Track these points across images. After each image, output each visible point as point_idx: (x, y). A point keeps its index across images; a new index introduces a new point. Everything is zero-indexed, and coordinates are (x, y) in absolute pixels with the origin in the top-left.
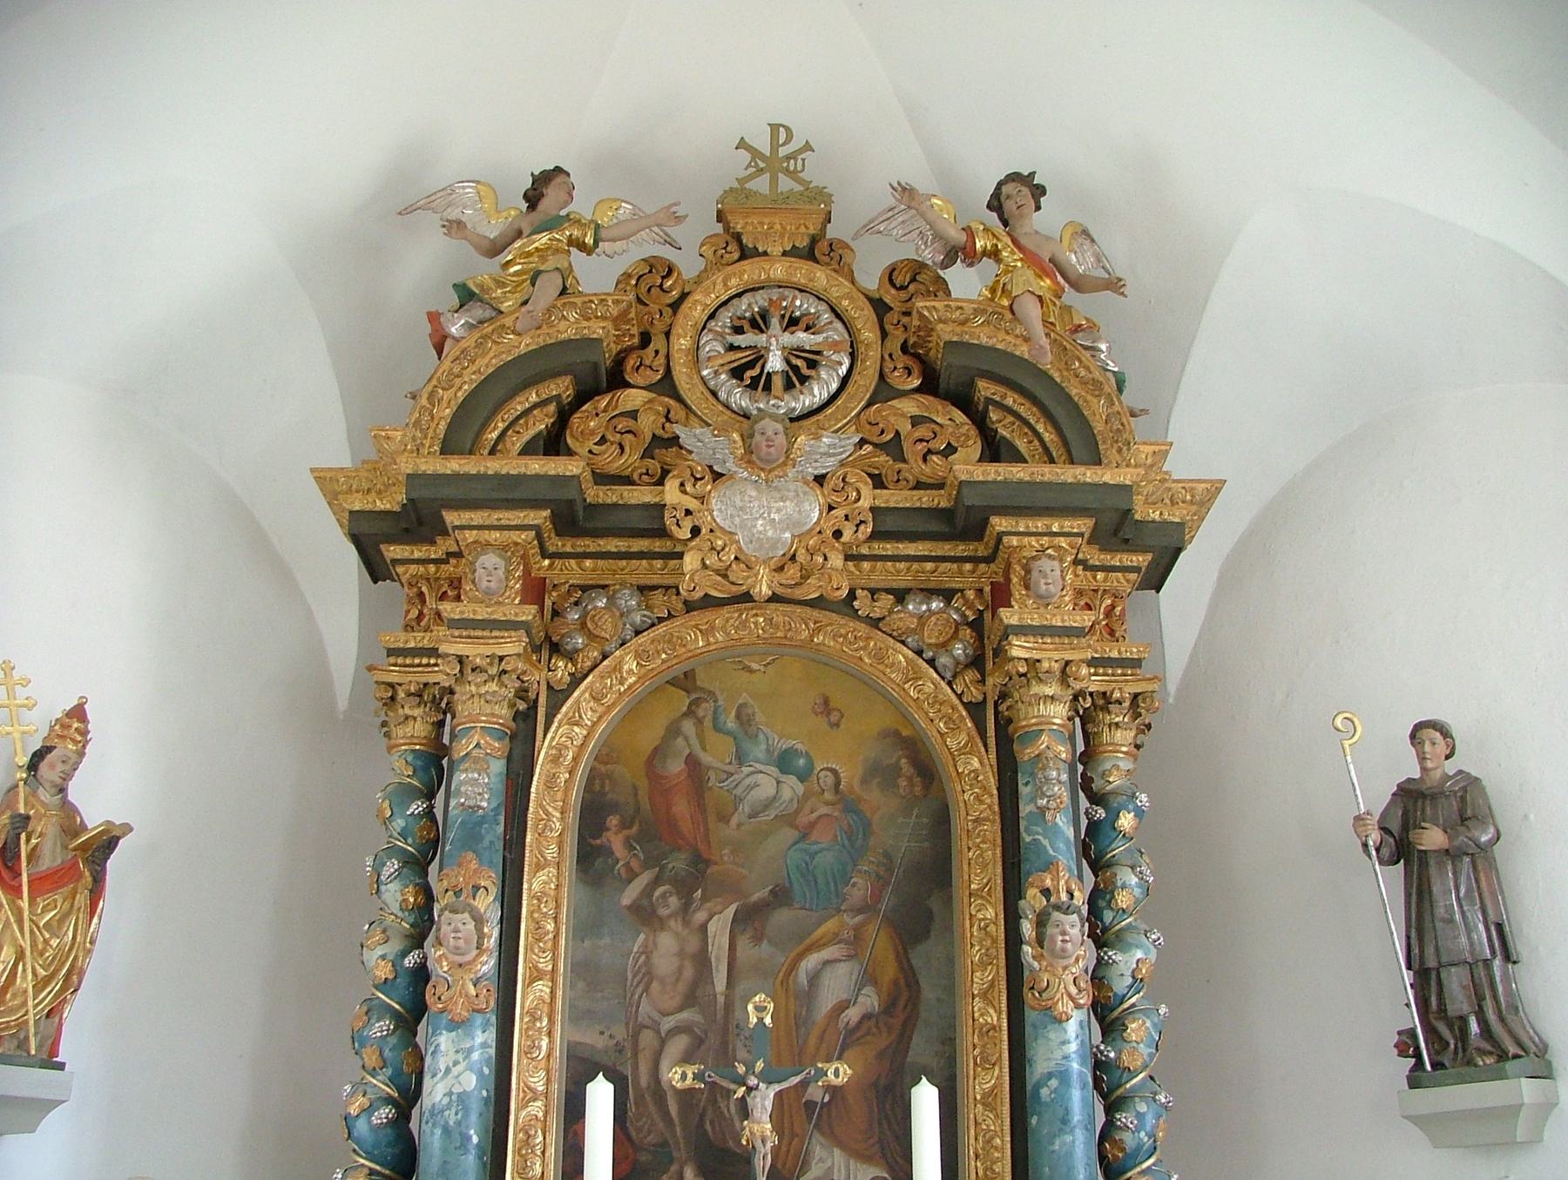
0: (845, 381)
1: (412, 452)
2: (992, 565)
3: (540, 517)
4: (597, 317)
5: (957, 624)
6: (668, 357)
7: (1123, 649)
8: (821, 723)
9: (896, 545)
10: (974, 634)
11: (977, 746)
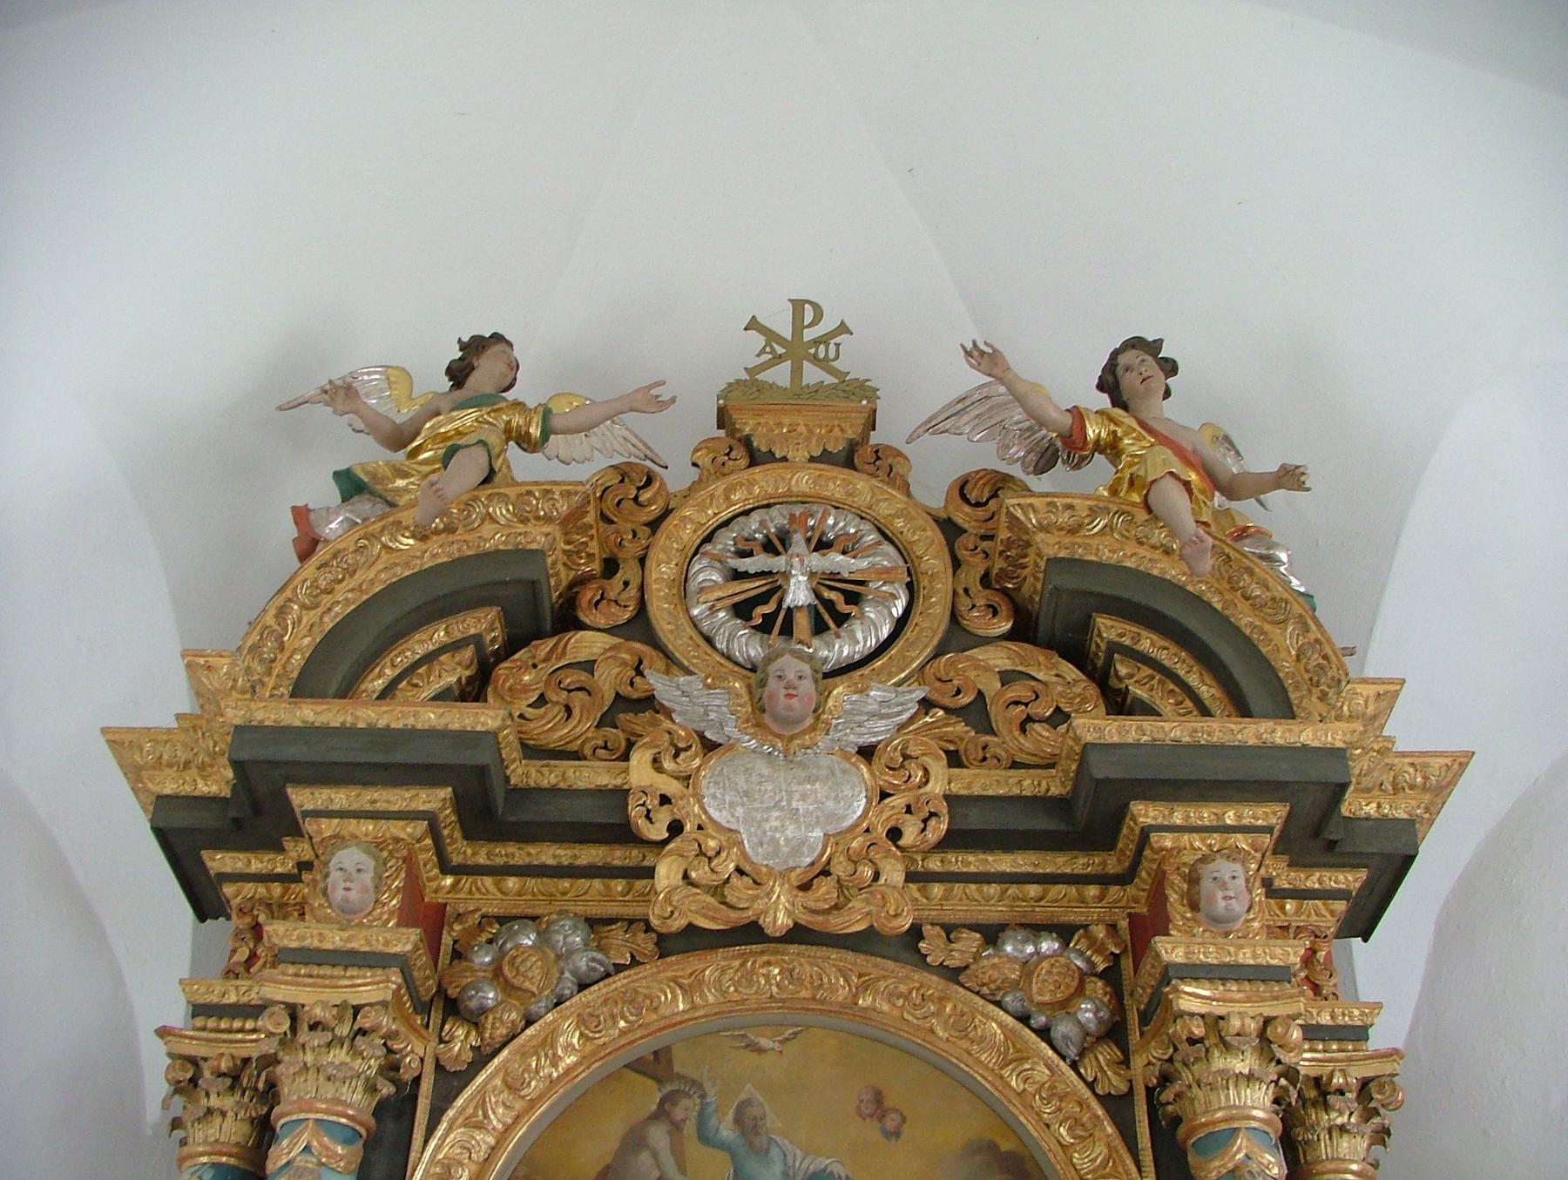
0: (901, 624)
1: (244, 692)
2: (1128, 888)
3: (434, 799)
4: (538, 518)
5: (1083, 976)
6: (642, 588)
7: (1338, 1011)
8: (871, 1130)
9: (982, 856)
10: (1108, 989)
11: (1123, 1162)
